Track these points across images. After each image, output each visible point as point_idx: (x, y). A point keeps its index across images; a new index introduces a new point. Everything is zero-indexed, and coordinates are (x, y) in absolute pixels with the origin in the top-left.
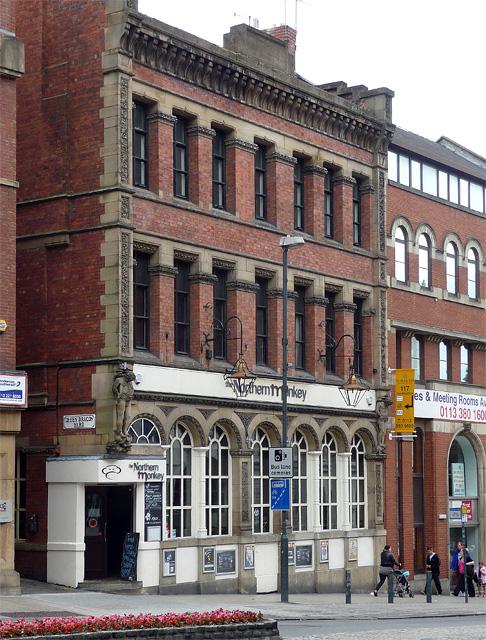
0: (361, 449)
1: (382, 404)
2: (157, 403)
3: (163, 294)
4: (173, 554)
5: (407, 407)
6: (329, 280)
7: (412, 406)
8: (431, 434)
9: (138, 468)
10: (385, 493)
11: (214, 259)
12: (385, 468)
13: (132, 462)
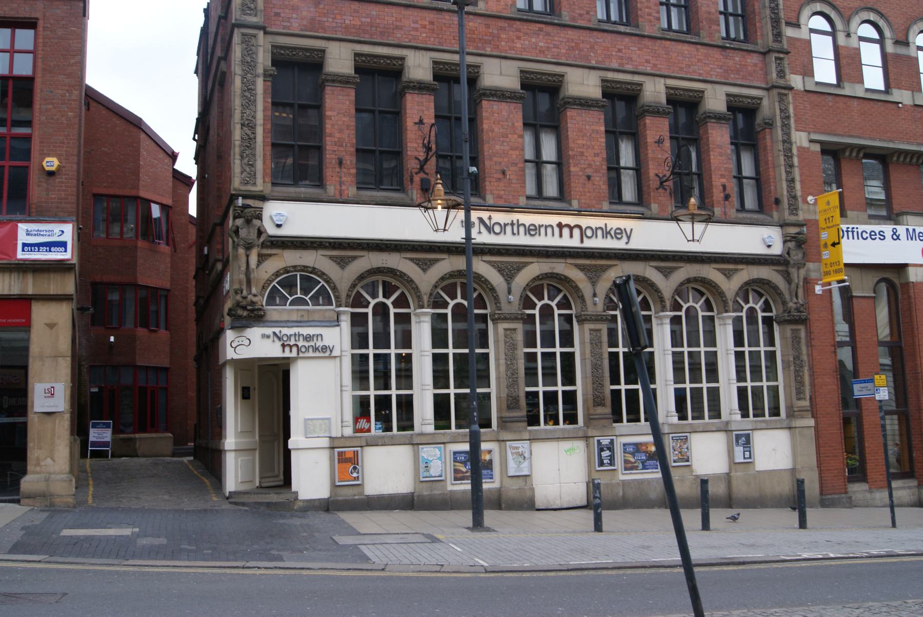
0: (562, 305)
1: (791, 245)
2: (321, 252)
3: (331, 110)
4: (748, 437)
5: (834, 245)
6: (671, 82)
7: (839, 243)
8: (907, 285)
9: (279, 339)
10: (811, 368)
11: (522, 72)
12: (809, 333)
13: (269, 331)
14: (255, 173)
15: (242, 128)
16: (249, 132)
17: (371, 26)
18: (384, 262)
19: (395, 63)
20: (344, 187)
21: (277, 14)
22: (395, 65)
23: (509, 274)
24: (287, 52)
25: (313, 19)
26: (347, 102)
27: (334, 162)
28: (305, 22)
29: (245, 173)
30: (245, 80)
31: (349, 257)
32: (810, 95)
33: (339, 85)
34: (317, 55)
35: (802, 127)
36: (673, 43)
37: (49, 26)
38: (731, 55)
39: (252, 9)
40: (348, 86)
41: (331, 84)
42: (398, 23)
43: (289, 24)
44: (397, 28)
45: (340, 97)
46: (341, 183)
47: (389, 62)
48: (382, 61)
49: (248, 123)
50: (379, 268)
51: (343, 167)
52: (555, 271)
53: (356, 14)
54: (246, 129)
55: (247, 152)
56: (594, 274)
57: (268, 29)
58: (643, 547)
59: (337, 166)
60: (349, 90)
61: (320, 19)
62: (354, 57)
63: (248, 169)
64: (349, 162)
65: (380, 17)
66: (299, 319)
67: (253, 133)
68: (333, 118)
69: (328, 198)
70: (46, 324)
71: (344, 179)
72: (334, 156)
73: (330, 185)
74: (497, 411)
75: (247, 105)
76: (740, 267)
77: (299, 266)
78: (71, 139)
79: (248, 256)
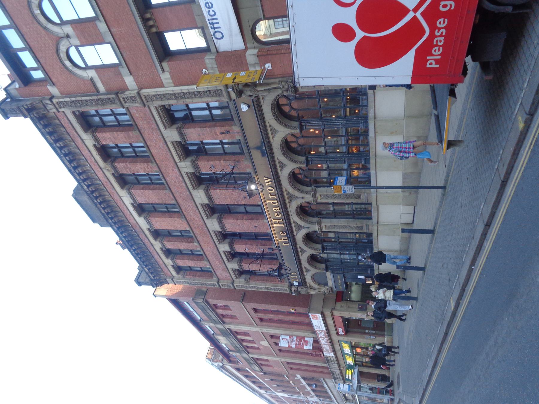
23: (300, 228)
32: (132, 71)
35: (158, 78)
36: (155, 158)
38: (141, 126)
52: (295, 212)
56: (292, 198)
58: (445, 165)
76: (268, 125)
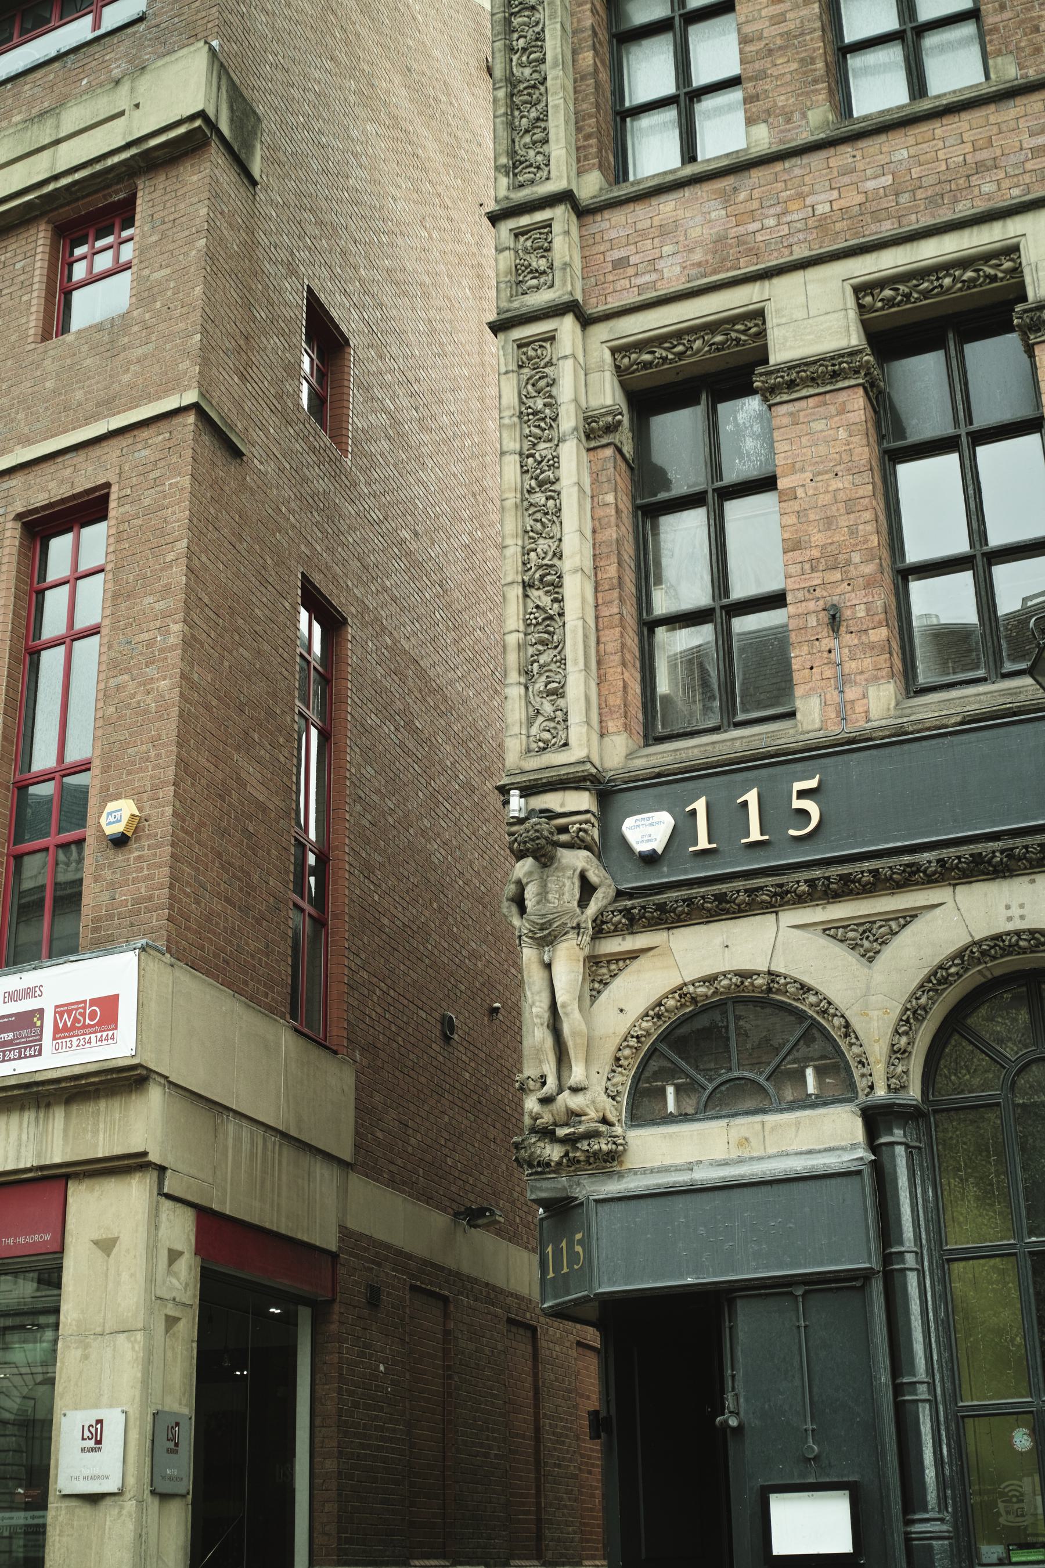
3: (793, 469)
14: (566, 714)
15: (526, 596)
16: (546, 601)
17: (897, 195)
18: (1015, 912)
19: (992, 272)
20: (851, 693)
21: (621, 264)
22: (994, 279)
24: (660, 352)
25: (720, 240)
26: (842, 434)
27: (812, 621)
28: (698, 256)
29: (541, 719)
30: (530, 460)
31: (887, 918)
33: (812, 391)
34: (743, 332)
37: (129, 492)
39: (544, 272)
40: (840, 385)
41: (785, 397)
42: (984, 155)
43: (654, 276)
44: (980, 168)
45: (818, 426)
46: (842, 682)
47: (969, 274)
48: (947, 281)
49: (542, 577)
50: (998, 937)
51: (843, 629)
53: (846, 180)
54: (540, 593)
55: (543, 659)
57: (594, 308)
59: (825, 631)
60: (843, 396)
61: (741, 230)
62: (858, 299)
63: (548, 708)
64: (861, 611)
65: (922, 158)
66: (734, 1154)
67: (555, 600)
68: (800, 492)
69: (802, 737)
70: (96, 1243)
71: (851, 666)
72: (811, 605)
73: (807, 696)
74: (293, 1491)
75: (539, 526)
77: (724, 974)
78: (163, 745)
79: (548, 966)
